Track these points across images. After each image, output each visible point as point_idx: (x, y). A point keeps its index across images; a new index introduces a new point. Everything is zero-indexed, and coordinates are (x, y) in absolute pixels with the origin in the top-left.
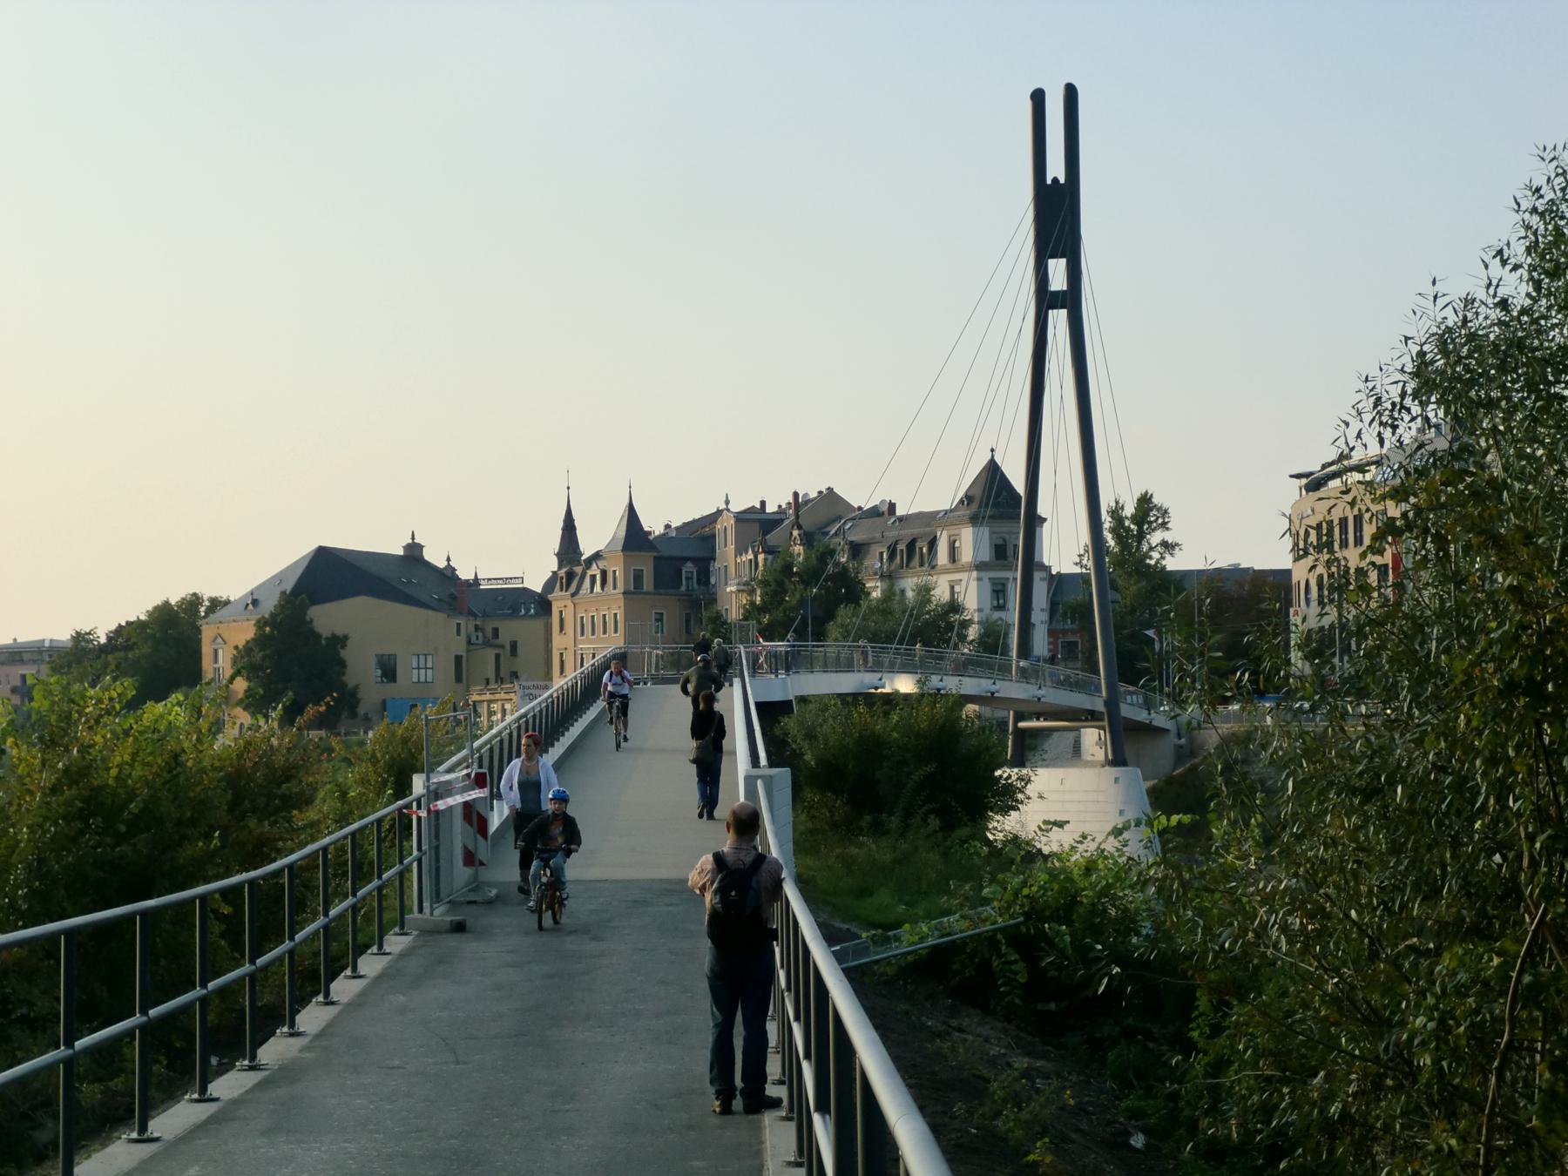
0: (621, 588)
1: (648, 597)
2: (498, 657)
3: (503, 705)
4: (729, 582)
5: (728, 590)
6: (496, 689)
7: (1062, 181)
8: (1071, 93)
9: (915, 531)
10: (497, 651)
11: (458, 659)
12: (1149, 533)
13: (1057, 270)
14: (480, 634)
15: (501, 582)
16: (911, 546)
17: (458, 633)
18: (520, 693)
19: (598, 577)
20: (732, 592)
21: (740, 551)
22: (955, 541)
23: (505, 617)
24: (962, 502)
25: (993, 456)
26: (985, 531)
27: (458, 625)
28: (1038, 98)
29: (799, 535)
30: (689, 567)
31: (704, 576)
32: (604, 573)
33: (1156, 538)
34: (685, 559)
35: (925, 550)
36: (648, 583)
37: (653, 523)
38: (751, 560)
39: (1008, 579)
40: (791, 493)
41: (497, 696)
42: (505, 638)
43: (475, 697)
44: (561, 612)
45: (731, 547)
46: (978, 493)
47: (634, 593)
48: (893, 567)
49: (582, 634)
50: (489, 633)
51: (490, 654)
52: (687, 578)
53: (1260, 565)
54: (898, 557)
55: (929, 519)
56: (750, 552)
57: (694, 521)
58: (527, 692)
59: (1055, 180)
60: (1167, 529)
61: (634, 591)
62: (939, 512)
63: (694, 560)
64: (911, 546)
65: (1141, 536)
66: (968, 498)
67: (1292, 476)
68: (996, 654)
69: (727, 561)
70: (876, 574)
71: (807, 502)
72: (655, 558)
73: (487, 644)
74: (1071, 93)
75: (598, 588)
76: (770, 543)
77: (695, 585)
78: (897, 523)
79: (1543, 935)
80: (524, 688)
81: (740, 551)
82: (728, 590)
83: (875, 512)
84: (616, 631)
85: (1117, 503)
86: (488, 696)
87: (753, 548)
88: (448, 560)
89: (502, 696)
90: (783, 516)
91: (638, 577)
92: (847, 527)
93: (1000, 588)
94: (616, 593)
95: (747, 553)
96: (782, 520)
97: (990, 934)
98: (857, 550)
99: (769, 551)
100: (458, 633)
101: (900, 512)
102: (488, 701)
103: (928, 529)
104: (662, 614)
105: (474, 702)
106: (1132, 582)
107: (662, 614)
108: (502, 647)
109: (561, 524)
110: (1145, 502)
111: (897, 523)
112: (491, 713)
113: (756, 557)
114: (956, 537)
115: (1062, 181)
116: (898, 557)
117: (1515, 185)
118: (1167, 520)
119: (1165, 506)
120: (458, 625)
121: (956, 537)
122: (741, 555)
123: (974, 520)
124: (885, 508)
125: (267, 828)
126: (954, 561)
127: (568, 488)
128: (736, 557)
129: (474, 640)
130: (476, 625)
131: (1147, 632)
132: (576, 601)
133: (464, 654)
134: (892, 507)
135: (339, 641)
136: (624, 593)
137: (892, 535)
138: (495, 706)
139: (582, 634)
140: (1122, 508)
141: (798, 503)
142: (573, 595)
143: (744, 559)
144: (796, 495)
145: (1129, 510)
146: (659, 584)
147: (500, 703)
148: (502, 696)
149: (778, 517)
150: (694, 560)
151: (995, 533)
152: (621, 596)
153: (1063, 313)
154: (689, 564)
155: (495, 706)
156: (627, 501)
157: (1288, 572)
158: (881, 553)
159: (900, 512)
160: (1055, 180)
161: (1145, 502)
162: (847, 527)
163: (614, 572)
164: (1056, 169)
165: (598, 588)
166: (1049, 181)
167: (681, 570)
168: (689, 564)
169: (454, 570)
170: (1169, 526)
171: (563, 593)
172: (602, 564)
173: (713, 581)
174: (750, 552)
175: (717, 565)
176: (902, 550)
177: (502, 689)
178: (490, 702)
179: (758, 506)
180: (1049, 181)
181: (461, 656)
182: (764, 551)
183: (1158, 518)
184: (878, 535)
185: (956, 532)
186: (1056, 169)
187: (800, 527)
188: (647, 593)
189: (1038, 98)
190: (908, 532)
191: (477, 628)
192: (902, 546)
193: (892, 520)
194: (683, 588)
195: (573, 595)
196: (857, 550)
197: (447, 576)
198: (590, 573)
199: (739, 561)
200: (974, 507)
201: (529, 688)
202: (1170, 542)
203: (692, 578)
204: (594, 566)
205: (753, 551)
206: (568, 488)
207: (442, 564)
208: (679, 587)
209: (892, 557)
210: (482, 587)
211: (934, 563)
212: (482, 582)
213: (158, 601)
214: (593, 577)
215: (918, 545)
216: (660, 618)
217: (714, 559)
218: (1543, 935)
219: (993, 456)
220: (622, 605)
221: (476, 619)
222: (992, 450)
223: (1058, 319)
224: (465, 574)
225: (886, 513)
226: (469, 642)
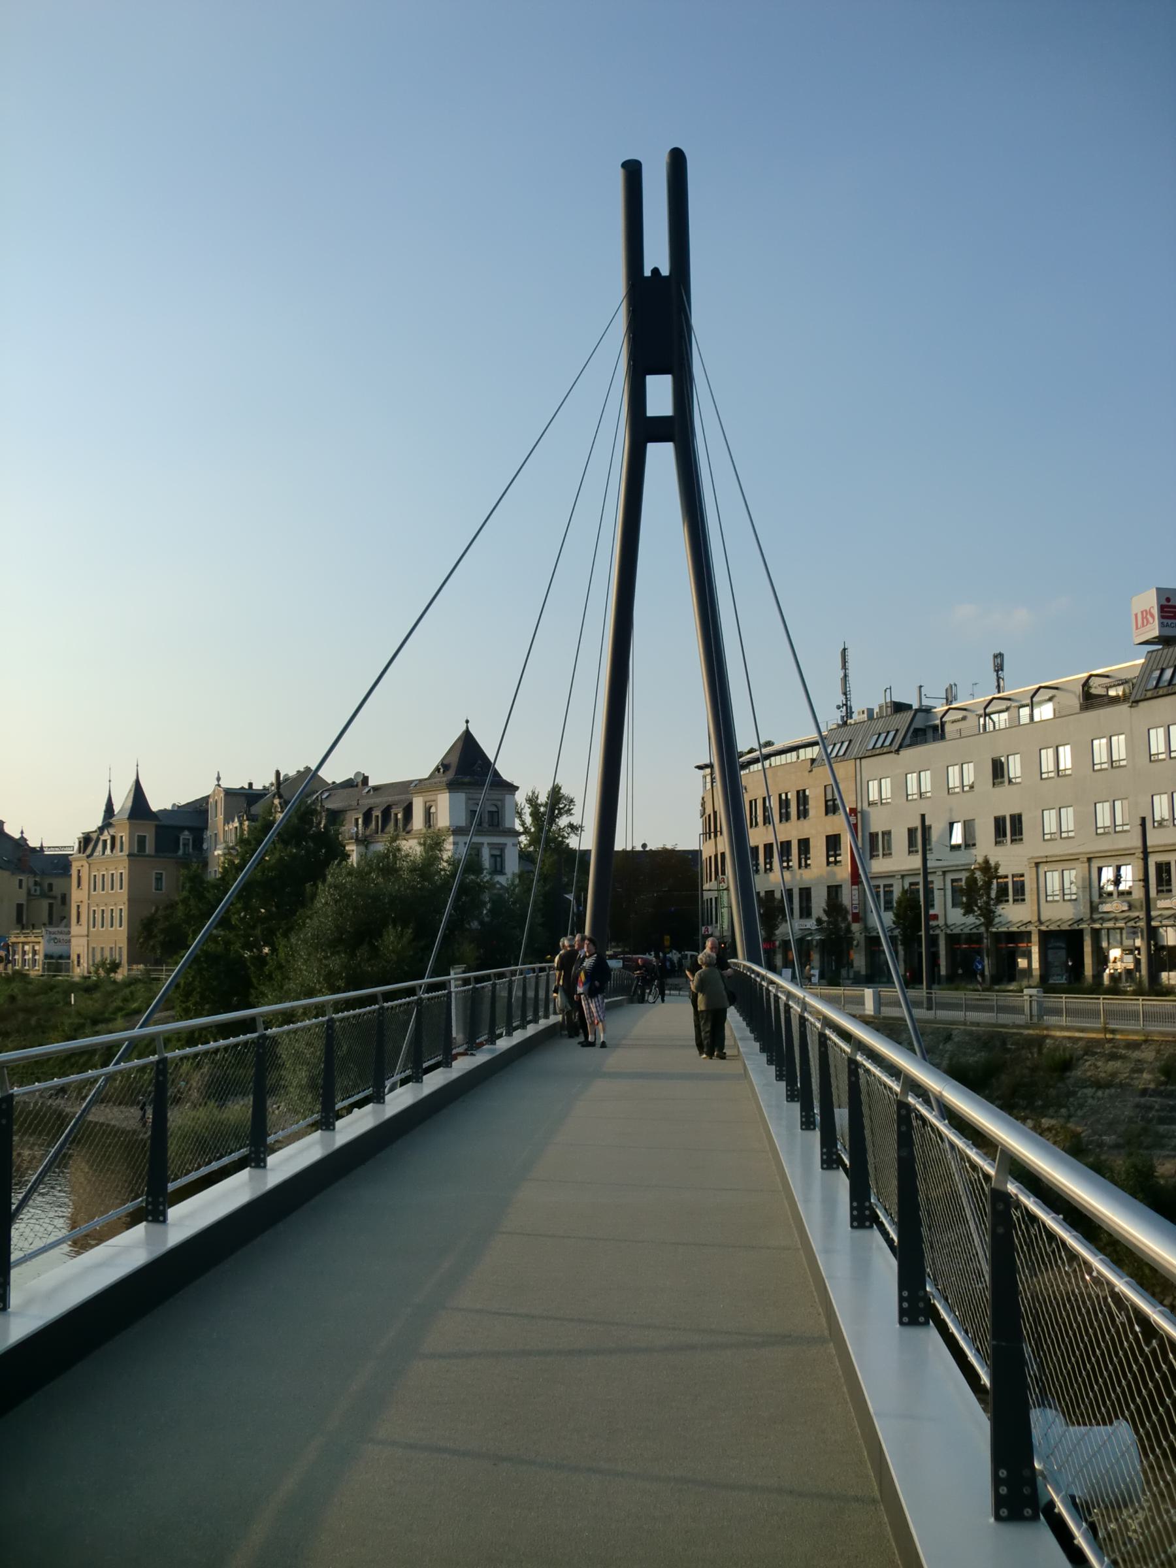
0: (126, 851)
1: (147, 859)
2: (51, 905)
3: (33, 947)
4: (218, 847)
5: (216, 853)
6: (28, 933)
8: (677, 161)
9: (390, 799)
10: (51, 901)
11: (20, 907)
12: (558, 818)
14: (38, 888)
15: (57, 849)
16: (386, 813)
17: (20, 887)
18: (46, 937)
19: (109, 842)
20: (219, 855)
21: (228, 819)
22: (430, 807)
23: (57, 875)
24: (437, 769)
25: (467, 728)
26: (461, 797)
27: (21, 881)
29: (280, 803)
30: (186, 834)
31: (198, 841)
32: (113, 838)
33: (563, 821)
34: (182, 829)
35: (400, 816)
36: (150, 848)
37: (158, 802)
38: (236, 828)
39: (483, 844)
40: (274, 772)
41: (29, 939)
42: (57, 891)
43: (13, 940)
44: (79, 871)
45: (221, 817)
46: (454, 761)
47: (138, 856)
48: (368, 833)
49: (95, 890)
50: (46, 886)
51: (45, 903)
52: (184, 845)
53: (681, 847)
54: (374, 823)
55: (405, 787)
56: (236, 820)
57: (197, 800)
58: (53, 936)
59: (656, 271)
60: (571, 814)
61: (137, 855)
62: (412, 782)
63: (190, 829)
64: (386, 813)
65: (552, 819)
66: (444, 766)
69: (218, 830)
70: (352, 838)
71: (287, 779)
72: (157, 827)
73: (43, 895)
74: (677, 161)
75: (108, 851)
76: (253, 813)
77: (191, 850)
78: (372, 792)
80: (50, 933)
81: (228, 819)
82: (216, 853)
83: (349, 784)
84: (121, 888)
85: (534, 793)
86: (22, 939)
87: (239, 817)
88: (22, 833)
89: (33, 939)
90: (267, 792)
91: (142, 841)
92: (324, 796)
93: (497, 852)
94: (122, 855)
95: (233, 821)
96: (266, 795)
98: (336, 817)
99: (252, 818)
100: (20, 887)
101: (372, 783)
102: (22, 943)
103: (403, 797)
104: (161, 874)
105: (13, 943)
106: (548, 855)
107: (161, 874)
108: (55, 898)
109: (104, 808)
110: (556, 793)
111: (372, 792)
112: (24, 953)
113: (241, 824)
114: (432, 803)
115: (665, 271)
116: (374, 823)
118: (572, 807)
119: (572, 796)
120: (21, 881)
121: (432, 803)
122: (228, 823)
123: (452, 786)
124: (360, 779)
126: (430, 826)
127: (110, 781)
128: (224, 825)
129: (32, 892)
130: (36, 881)
131: (567, 896)
132: (90, 862)
133: (24, 902)
134: (365, 780)
135: (766, 892)
136: (128, 856)
137: (367, 803)
138: (27, 948)
139: (95, 890)
140: (537, 798)
141: (280, 782)
142: (88, 857)
143: (231, 827)
144: (278, 773)
145: (543, 799)
146: (159, 848)
147: (31, 945)
148: (33, 939)
149: (264, 792)
150: (190, 829)
151: (470, 799)
152: (126, 858)
154: (186, 833)
155: (27, 948)
156: (134, 778)
157: (696, 854)
158: (357, 820)
159: (372, 783)
160: (656, 271)
161: (556, 793)
162: (324, 796)
163: (122, 837)
164: (657, 258)
165: (108, 851)
166: (647, 273)
167: (179, 839)
168: (186, 833)
169: (26, 840)
170: (572, 812)
171: (81, 855)
172: (112, 831)
173: (205, 846)
174: (236, 820)
175: (209, 833)
176: (377, 816)
177: (33, 933)
178: (24, 943)
179: (247, 787)
180: (647, 273)
181: (22, 905)
182: (248, 819)
183: (566, 805)
184: (354, 803)
185: (432, 798)
186: (657, 258)
187: (280, 797)
188: (149, 856)
190: (381, 801)
191: (36, 883)
192: (377, 813)
193: (367, 790)
194: (181, 852)
195: (88, 857)
196: (336, 817)
197: (21, 843)
198: (102, 838)
199: (226, 828)
200: (451, 774)
201: (54, 933)
202: (575, 824)
203: (188, 845)
204: (106, 833)
205: (239, 820)
206: (110, 781)
207: (17, 836)
208: (177, 852)
209: (367, 821)
210: (46, 853)
211: (409, 828)
212: (45, 849)
214: (105, 842)
215: (393, 811)
216: (159, 879)
217: (206, 828)
219: (467, 728)
220: (127, 865)
221: (35, 876)
222: (467, 722)
224: (33, 843)
225: (360, 784)
226: (29, 893)
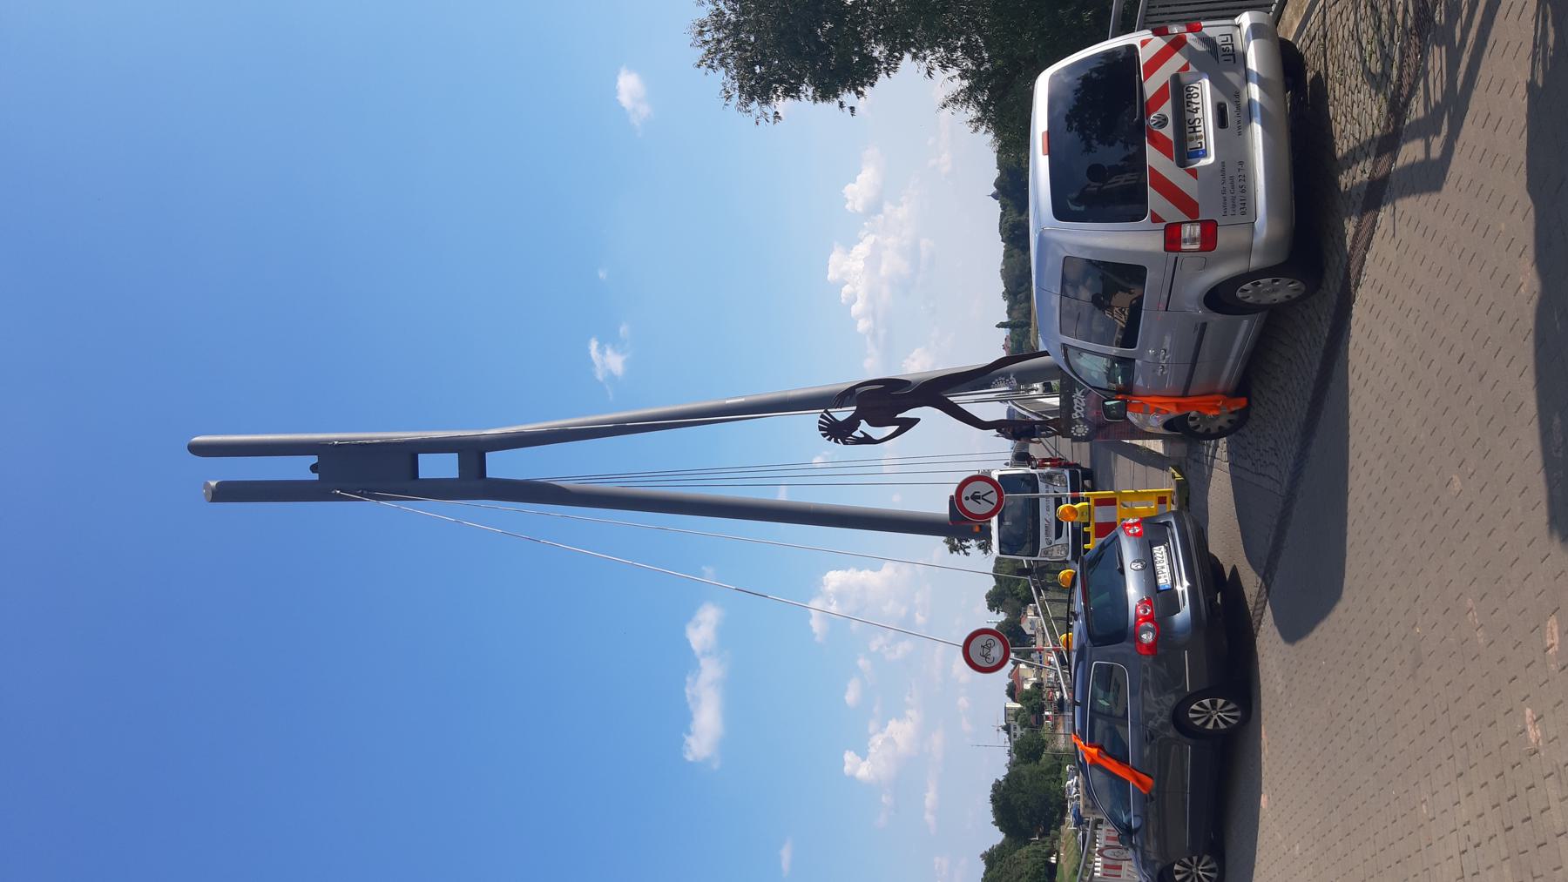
7: (314, 459)
13: (436, 467)
28: (227, 492)
59: (314, 468)
67: (998, 326)
68: (1071, 491)
79: (1202, 717)
97: (1045, 564)
117: (999, 269)
125: (1164, 570)
153: (491, 457)
160: (314, 468)
164: (300, 469)
166: (316, 477)
180: (316, 477)
189: (227, 492)
213: (989, 792)
218: (1202, 717)
223: (499, 465)
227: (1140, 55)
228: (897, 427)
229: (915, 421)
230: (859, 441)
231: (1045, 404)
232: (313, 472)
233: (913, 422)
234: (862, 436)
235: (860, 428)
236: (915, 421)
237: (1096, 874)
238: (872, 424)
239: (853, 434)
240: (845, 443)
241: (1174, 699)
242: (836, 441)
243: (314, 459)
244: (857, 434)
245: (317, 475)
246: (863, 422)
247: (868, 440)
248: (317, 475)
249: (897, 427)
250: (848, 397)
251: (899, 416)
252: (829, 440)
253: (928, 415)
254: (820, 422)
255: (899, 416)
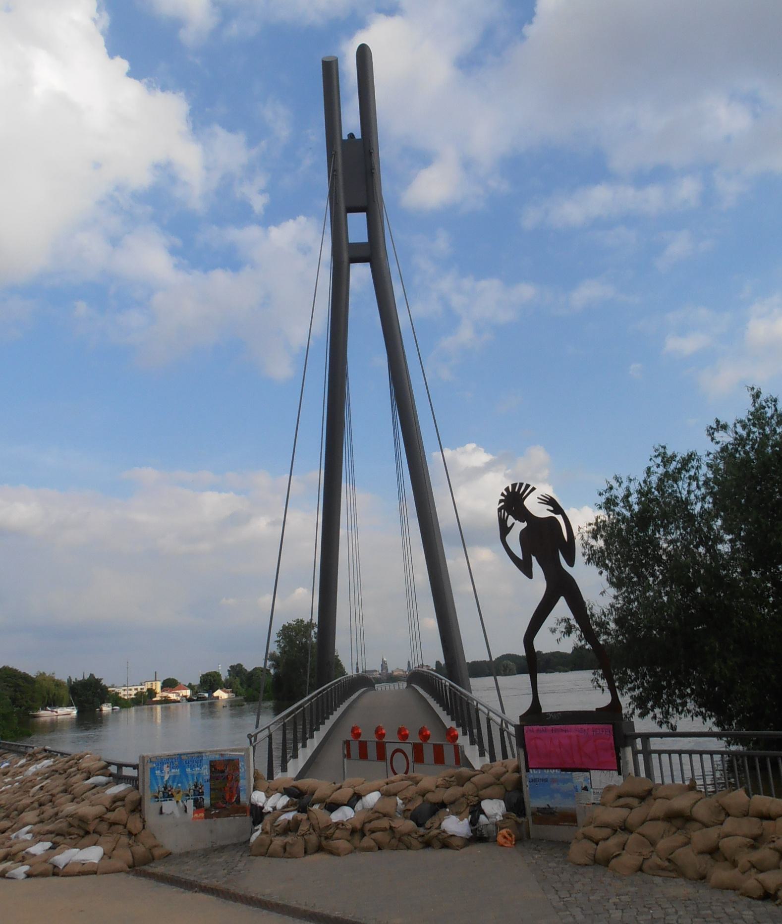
7: (358, 136)
59: (351, 136)
160: (351, 136)
164: (351, 122)
166: (345, 137)
180: (345, 137)
227: (621, 765)
228: (521, 558)
229: (529, 575)
230: (502, 522)
231: (87, 784)
232: (348, 135)
233: (529, 573)
234: (509, 525)
235: (517, 522)
236: (529, 575)
237: (301, 727)
238: (524, 535)
239: (510, 517)
240: (500, 510)
241: (206, 766)
242: (501, 501)
243: (358, 136)
244: (511, 520)
245: (347, 138)
246: (525, 524)
247: (505, 530)
248: (347, 138)
249: (521, 558)
250: (552, 508)
251: (534, 559)
252: (503, 494)
253: (538, 584)
254: (521, 484)
255: (534, 559)
